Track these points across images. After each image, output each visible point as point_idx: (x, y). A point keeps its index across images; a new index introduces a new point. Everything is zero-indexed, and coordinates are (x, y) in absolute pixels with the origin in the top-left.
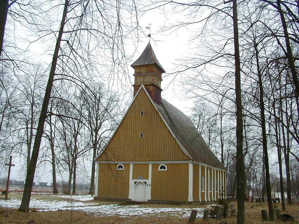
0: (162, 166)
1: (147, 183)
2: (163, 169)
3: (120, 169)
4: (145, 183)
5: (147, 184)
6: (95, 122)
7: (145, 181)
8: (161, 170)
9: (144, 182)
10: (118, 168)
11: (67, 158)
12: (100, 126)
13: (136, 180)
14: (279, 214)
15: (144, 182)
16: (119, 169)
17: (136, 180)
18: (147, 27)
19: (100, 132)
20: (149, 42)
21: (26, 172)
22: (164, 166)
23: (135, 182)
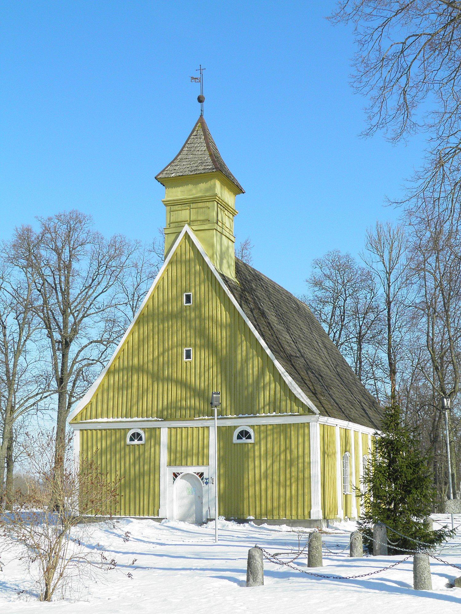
0: (133, 435)
1: (205, 476)
2: (136, 440)
3: (136, 442)
4: (201, 475)
5: (206, 479)
6: (60, 319)
7: (200, 469)
8: (240, 441)
9: (198, 474)
10: (131, 439)
11: (367, 373)
12: (75, 331)
13: (176, 470)
14: (418, 513)
15: (198, 474)
16: (133, 443)
17: (176, 470)
18: (193, 78)
19: (74, 348)
20: (201, 116)
21: (314, 581)
22: (138, 434)
23: (174, 474)
